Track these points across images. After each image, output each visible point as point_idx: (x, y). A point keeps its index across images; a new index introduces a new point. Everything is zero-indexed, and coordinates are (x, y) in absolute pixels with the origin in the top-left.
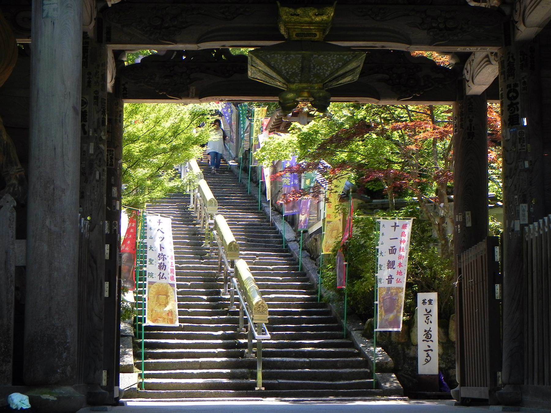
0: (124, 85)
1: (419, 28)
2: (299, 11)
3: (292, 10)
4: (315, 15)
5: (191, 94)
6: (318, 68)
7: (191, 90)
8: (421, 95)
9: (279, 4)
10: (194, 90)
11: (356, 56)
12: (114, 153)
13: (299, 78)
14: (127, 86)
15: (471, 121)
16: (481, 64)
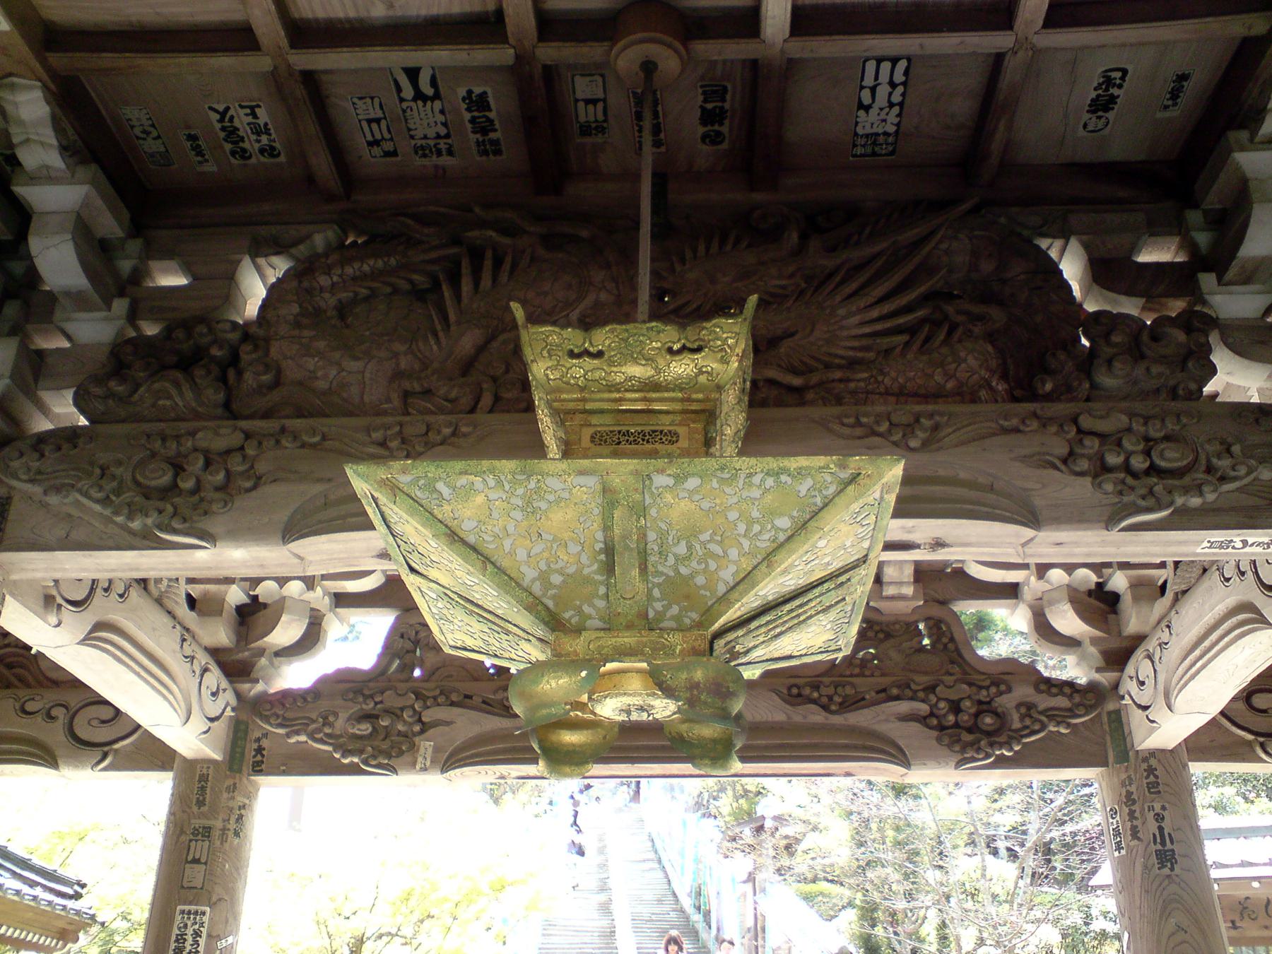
0: (258, 740)
1: (1058, 469)
2: (603, 338)
3: (572, 337)
5: (420, 759)
6: (682, 549)
7: (422, 750)
8: (1016, 752)
9: (518, 311)
10: (430, 750)
11: (854, 479)
12: (206, 919)
13: (601, 604)
15: (1159, 818)
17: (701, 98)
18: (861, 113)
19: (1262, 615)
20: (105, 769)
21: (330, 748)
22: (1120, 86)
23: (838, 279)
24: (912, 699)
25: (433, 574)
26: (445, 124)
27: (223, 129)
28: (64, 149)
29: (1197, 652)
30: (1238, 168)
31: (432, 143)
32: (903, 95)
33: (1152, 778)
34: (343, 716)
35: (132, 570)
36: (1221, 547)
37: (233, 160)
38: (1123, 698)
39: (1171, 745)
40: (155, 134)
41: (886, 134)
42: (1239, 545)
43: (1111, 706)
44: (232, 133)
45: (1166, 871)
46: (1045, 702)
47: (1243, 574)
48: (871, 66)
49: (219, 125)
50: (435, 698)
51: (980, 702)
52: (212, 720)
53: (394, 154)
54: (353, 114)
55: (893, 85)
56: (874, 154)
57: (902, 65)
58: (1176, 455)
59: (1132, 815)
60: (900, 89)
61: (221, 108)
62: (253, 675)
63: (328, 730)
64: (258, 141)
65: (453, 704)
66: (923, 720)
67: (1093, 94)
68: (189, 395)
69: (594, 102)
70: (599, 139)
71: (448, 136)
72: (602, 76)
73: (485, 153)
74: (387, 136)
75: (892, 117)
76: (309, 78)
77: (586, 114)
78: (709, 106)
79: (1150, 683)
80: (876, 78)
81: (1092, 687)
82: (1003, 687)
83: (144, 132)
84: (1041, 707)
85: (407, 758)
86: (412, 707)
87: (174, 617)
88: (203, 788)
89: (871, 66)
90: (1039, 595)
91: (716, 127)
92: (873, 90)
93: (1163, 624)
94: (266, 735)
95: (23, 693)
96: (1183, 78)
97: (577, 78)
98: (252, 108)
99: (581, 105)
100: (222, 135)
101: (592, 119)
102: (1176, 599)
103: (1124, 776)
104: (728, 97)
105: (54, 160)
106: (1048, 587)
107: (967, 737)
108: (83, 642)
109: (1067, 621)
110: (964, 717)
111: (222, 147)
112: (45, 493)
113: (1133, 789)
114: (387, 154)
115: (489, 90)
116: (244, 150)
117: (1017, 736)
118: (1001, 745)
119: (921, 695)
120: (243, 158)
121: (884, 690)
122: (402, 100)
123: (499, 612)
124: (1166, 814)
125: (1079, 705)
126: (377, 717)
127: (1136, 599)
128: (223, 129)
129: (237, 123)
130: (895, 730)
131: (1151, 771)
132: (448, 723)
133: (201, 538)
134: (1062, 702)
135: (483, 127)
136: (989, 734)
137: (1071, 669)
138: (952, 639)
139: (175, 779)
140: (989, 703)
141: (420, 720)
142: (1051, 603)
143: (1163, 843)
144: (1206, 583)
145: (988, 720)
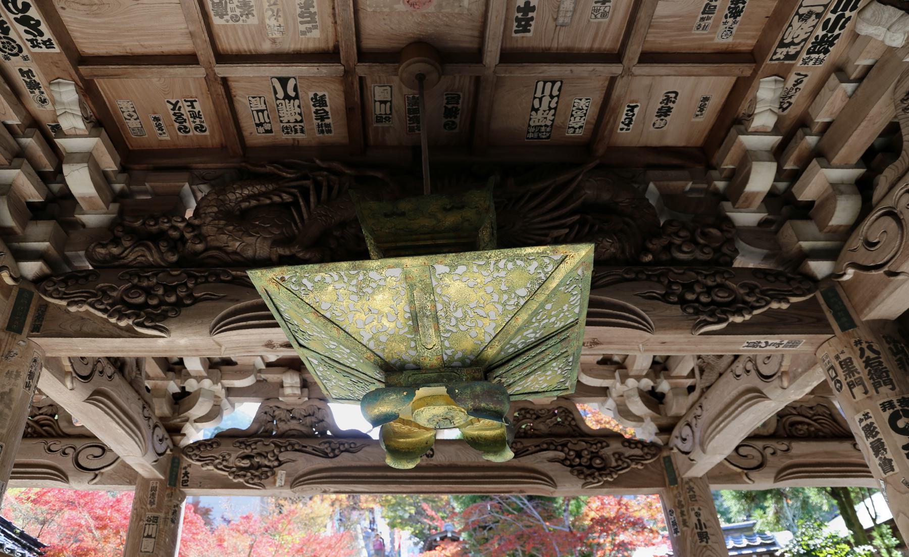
0: (185, 468)
4: (445, 209)
5: (278, 481)
7: (279, 475)
14: (189, 470)
15: (698, 515)
16: (717, 422)
17: (445, 101)
18: (534, 113)
19: (762, 393)
20: (96, 484)
21: (226, 474)
22: (674, 102)
23: (526, 198)
24: (556, 450)
25: (311, 345)
26: (300, 114)
27: (175, 114)
28: (86, 119)
29: (721, 419)
30: (741, 144)
31: (292, 125)
32: (557, 103)
33: (692, 493)
34: (234, 456)
35: (119, 351)
36: (754, 346)
37: (179, 134)
38: (672, 449)
39: (700, 475)
40: (135, 117)
41: (546, 126)
42: (763, 345)
43: (665, 454)
44: (179, 117)
45: (704, 544)
46: (628, 452)
47: (748, 371)
48: (541, 84)
49: (172, 112)
50: (286, 447)
51: (592, 452)
52: (159, 455)
53: (270, 131)
54: (247, 106)
55: (552, 97)
56: (539, 138)
57: (558, 84)
58: (726, 295)
59: (682, 513)
60: (556, 99)
61: (174, 101)
62: (182, 432)
63: (225, 463)
64: (194, 122)
65: (296, 450)
66: (562, 462)
67: (660, 106)
68: (156, 256)
69: (385, 102)
70: (386, 125)
71: (301, 121)
72: (391, 87)
73: (322, 132)
74: (267, 121)
75: (550, 117)
76: (225, 81)
77: (379, 109)
78: (450, 106)
79: (690, 439)
80: (543, 93)
81: (653, 445)
82: (604, 444)
83: (130, 115)
84: (627, 455)
85: (271, 479)
86: (273, 451)
87: (139, 394)
88: (153, 495)
89: (541, 84)
90: (621, 393)
91: (453, 119)
92: (541, 99)
93: (697, 406)
94: (190, 465)
95: (50, 442)
96: (706, 99)
97: (377, 88)
98: (192, 102)
99: (378, 104)
100: (174, 118)
101: (383, 112)
102: (703, 393)
103: (675, 492)
104: (460, 101)
105: (80, 124)
106: (626, 389)
107: (587, 472)
108: (88, 400)
109: (638, 407)
110: (584, 460)
111: (173, 125)
112: (68, 305)
113: (682, 499)
114: (267, 131)
115: (326, 94)
116: (186, 127)
117: (617, 469)
118: (606, 475)
119: (560, 448)
120: (185, 132)
121: (538, 446)
122: (277, 99)
123: (353, 366)
124: (701, 512)
125: (647, 454)
126: (253, 457)
127: (676, 395)
128: (175, 114)
129: (182, 111)
130: (546, 467)
131: (691, 489)
132: (294, 461)
133: (162, 331)
134: (638, 452)
135: (322, 117)
136: (599, 470)
137: (645, 432)
138: (573, 419)
139: (136, 489)
140: (597, 453)
141: (277, 459)
142: (629, 397)
143: (701, 528)
144: (724, 379)
145: (598, 461)
